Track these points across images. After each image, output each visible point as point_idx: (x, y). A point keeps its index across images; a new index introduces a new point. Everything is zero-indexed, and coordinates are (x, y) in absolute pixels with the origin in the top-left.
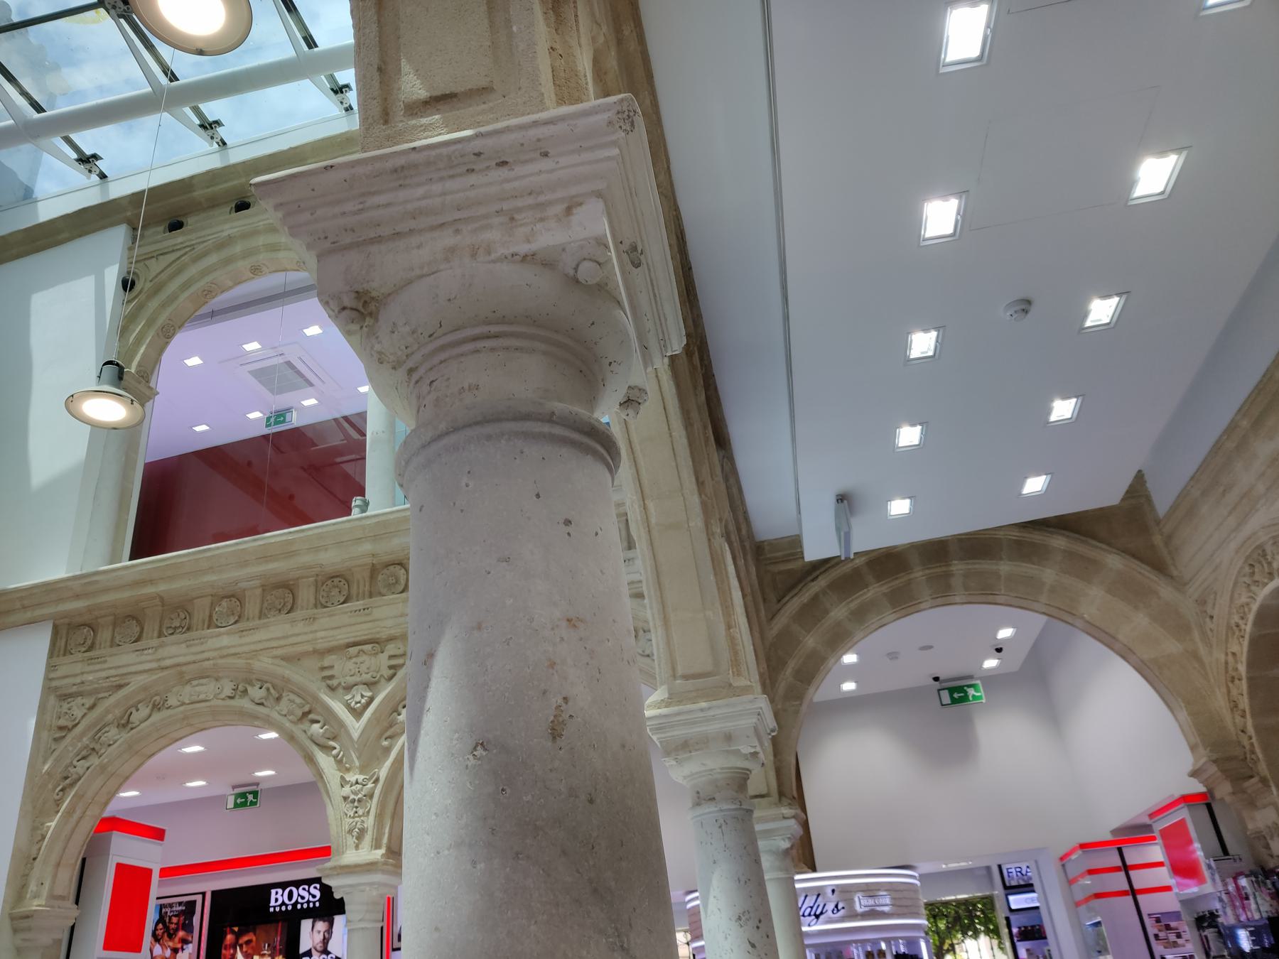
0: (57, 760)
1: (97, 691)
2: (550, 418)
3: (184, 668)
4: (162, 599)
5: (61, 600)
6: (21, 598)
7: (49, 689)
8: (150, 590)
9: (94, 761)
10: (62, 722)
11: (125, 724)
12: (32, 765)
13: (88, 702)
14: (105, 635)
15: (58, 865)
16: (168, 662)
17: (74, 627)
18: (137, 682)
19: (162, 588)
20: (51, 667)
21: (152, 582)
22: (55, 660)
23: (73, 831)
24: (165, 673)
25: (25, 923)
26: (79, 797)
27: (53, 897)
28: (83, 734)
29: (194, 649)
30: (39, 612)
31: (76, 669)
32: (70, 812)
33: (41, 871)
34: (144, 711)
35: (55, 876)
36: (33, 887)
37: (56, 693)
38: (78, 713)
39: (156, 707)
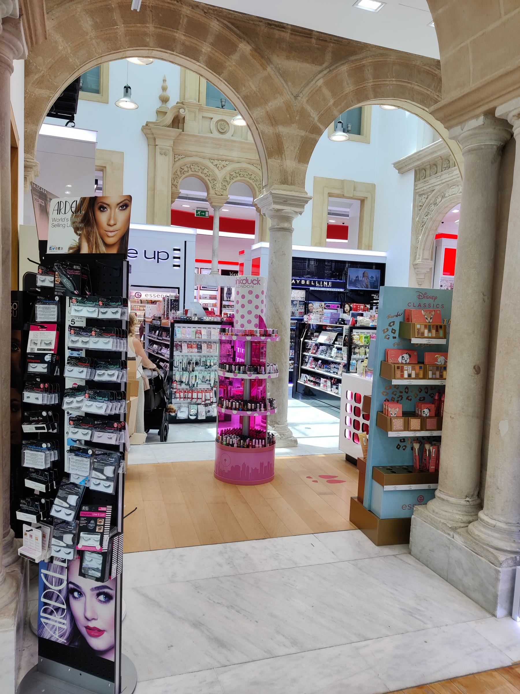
0: (420, 217)
1: (428, 193)
2: (275, 229)
3: (448, 183)
4: (441, 157)
5: (414, 162)
6: (404, 163)
7: (415, 193)
8: (435, 155)
9: (429, 216)
10: (420, 204)
11: (435, 204)
12: (413, 219)
13: (426, 196)
14: (428, 172)
15: (424, 249)
16: (444, 181)
17: (420, 170)
18: (437, 188)
19: (439, 154)
20: (415, 185)
21: (435, 152)
22: (416, 183)
23: (426, 239)
24: (444, 185)
25: (416, 267)
26: (426, 228)
27: (423, 259)
28: (425, 208)
29: (450, 175)
30: (410, 167)
31: (423, 186)
32: (424, 234)
33: (420, 251)
34: (440, 199)
35: (423, 253)
36: (418, 256)
37: (418, 194)
38: (424, 200)
39: (443, 197)
